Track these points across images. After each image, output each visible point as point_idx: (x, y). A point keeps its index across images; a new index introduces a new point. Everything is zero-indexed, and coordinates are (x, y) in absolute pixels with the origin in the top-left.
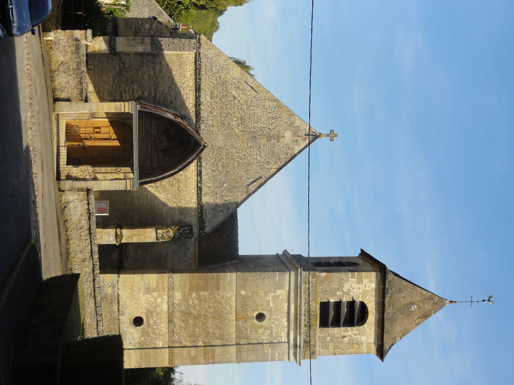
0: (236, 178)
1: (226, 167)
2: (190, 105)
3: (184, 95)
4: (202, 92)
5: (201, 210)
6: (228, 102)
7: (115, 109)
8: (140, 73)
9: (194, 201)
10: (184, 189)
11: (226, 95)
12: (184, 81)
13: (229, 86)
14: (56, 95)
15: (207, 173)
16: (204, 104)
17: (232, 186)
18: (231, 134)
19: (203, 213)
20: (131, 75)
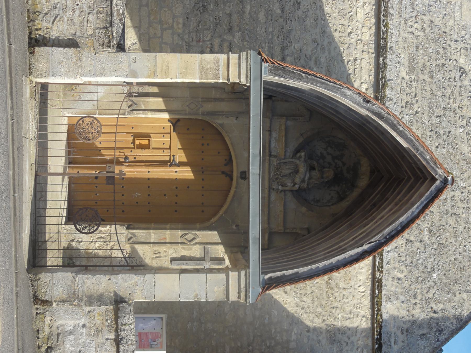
0: (460, 259)
1: (438, 234)
2: (363, 84)
3: (348, 62)
4: (389, 56)
5: (380, 334)
6: (447, 83)
7: (201, 72)
8: (248, 7)
9: (362, 312)
10: (342, 285)
11: (443, 65)
12: (349, 30)
13: (452, 44)
14: (37, 30)
15: (396, 247)
16: (394, 85)
17: (449, 278)
18: (453, 157)
19: (382, 342)
20: (228, 12)
